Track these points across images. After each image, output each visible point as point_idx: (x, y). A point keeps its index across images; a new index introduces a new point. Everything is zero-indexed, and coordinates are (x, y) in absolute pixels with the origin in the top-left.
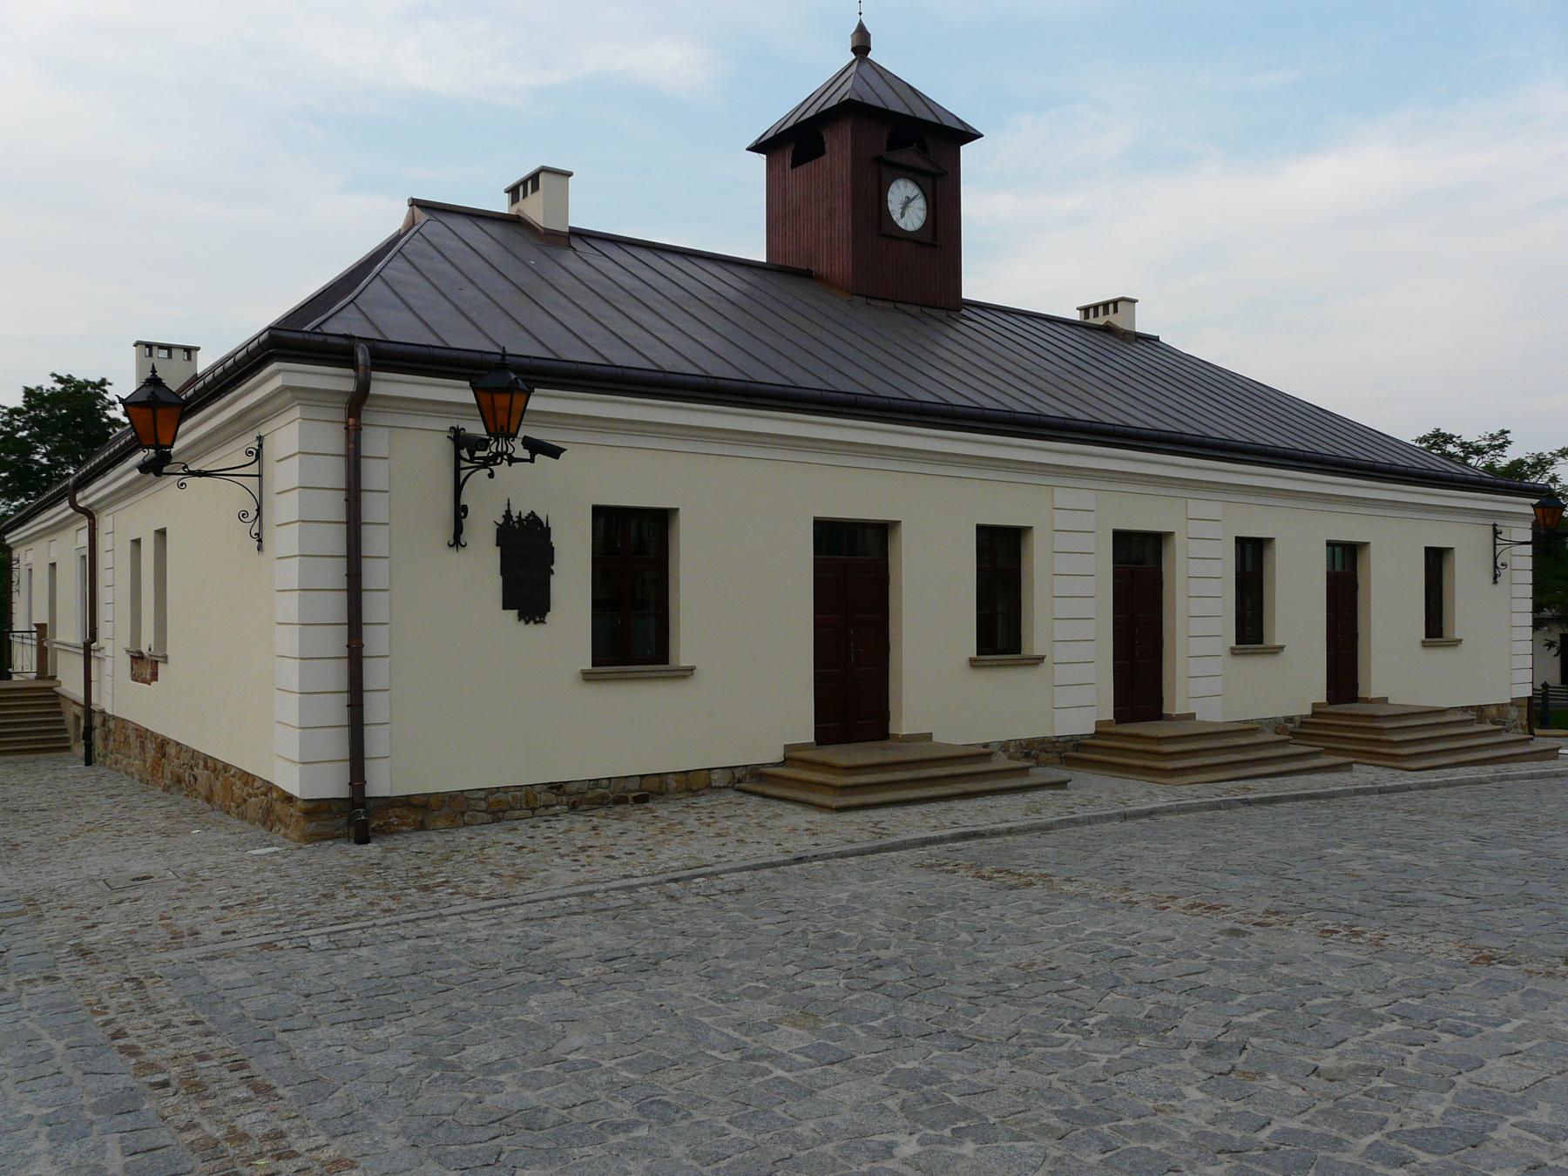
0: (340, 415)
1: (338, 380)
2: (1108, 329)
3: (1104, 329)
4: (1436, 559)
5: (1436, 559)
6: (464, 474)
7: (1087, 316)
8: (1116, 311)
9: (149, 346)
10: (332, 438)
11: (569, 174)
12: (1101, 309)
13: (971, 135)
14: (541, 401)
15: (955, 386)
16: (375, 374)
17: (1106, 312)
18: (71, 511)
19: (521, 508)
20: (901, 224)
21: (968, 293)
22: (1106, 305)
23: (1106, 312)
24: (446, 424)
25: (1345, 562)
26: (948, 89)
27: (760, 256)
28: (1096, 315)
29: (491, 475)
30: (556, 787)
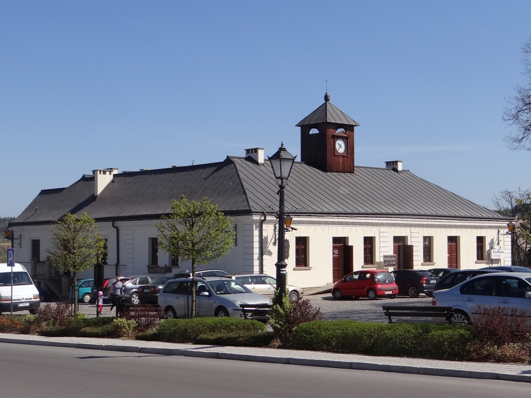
17: (393, 164)
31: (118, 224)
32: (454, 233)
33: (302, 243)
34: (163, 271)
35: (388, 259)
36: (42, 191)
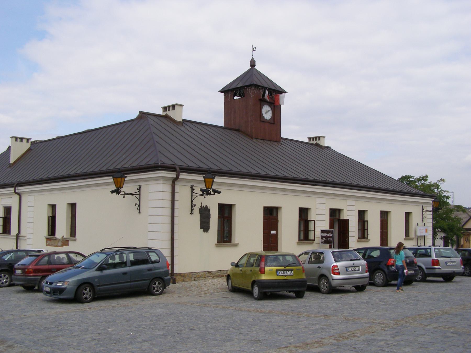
0: (171, 182)
1: (172, 175)
2: (317, 145)
3: (315, 145)
4: (408, 215)
5: (408, 215)
6: (194, 197)
7: (310, 140)
8: (319, 140)
9: (16, 138)
10: (169, 188)
11: (183, 105)
12: (315, 139)
13: (283, 92)
14: (218, 179)
15: (214, 132)
16: (180, 173)
17: (316, 140)
18: (13, 191)
19: (204, 204)
20: (264, 115)
21: (282, 136)
22: (316, 138)
23: (316, 140)
24: (190, 184)
25: (385, 215)
26: (277, 77)
27: (222, 124)
28: (313, 140)
29: (205, 198)
30: (210, 272)
31: (21, 189)
32: (385, 208)
33: (226, 211)
34: (60, 244)
35: (326, 235)
36: (201, 228)
